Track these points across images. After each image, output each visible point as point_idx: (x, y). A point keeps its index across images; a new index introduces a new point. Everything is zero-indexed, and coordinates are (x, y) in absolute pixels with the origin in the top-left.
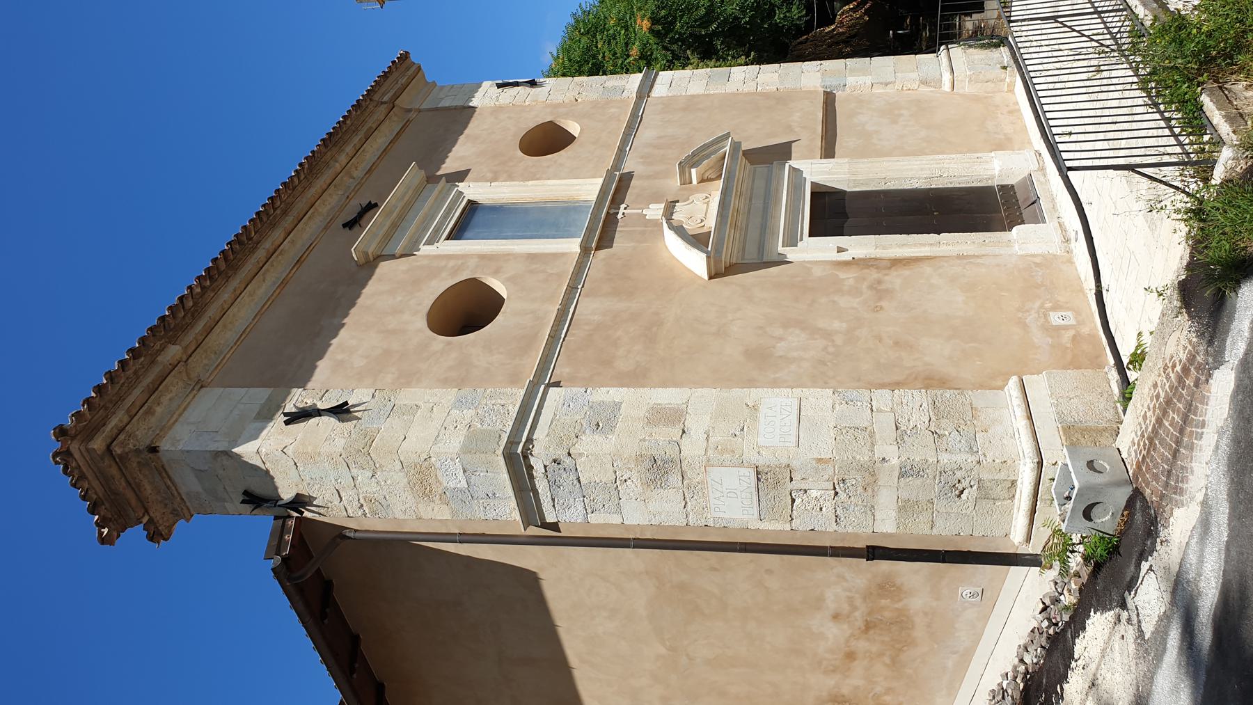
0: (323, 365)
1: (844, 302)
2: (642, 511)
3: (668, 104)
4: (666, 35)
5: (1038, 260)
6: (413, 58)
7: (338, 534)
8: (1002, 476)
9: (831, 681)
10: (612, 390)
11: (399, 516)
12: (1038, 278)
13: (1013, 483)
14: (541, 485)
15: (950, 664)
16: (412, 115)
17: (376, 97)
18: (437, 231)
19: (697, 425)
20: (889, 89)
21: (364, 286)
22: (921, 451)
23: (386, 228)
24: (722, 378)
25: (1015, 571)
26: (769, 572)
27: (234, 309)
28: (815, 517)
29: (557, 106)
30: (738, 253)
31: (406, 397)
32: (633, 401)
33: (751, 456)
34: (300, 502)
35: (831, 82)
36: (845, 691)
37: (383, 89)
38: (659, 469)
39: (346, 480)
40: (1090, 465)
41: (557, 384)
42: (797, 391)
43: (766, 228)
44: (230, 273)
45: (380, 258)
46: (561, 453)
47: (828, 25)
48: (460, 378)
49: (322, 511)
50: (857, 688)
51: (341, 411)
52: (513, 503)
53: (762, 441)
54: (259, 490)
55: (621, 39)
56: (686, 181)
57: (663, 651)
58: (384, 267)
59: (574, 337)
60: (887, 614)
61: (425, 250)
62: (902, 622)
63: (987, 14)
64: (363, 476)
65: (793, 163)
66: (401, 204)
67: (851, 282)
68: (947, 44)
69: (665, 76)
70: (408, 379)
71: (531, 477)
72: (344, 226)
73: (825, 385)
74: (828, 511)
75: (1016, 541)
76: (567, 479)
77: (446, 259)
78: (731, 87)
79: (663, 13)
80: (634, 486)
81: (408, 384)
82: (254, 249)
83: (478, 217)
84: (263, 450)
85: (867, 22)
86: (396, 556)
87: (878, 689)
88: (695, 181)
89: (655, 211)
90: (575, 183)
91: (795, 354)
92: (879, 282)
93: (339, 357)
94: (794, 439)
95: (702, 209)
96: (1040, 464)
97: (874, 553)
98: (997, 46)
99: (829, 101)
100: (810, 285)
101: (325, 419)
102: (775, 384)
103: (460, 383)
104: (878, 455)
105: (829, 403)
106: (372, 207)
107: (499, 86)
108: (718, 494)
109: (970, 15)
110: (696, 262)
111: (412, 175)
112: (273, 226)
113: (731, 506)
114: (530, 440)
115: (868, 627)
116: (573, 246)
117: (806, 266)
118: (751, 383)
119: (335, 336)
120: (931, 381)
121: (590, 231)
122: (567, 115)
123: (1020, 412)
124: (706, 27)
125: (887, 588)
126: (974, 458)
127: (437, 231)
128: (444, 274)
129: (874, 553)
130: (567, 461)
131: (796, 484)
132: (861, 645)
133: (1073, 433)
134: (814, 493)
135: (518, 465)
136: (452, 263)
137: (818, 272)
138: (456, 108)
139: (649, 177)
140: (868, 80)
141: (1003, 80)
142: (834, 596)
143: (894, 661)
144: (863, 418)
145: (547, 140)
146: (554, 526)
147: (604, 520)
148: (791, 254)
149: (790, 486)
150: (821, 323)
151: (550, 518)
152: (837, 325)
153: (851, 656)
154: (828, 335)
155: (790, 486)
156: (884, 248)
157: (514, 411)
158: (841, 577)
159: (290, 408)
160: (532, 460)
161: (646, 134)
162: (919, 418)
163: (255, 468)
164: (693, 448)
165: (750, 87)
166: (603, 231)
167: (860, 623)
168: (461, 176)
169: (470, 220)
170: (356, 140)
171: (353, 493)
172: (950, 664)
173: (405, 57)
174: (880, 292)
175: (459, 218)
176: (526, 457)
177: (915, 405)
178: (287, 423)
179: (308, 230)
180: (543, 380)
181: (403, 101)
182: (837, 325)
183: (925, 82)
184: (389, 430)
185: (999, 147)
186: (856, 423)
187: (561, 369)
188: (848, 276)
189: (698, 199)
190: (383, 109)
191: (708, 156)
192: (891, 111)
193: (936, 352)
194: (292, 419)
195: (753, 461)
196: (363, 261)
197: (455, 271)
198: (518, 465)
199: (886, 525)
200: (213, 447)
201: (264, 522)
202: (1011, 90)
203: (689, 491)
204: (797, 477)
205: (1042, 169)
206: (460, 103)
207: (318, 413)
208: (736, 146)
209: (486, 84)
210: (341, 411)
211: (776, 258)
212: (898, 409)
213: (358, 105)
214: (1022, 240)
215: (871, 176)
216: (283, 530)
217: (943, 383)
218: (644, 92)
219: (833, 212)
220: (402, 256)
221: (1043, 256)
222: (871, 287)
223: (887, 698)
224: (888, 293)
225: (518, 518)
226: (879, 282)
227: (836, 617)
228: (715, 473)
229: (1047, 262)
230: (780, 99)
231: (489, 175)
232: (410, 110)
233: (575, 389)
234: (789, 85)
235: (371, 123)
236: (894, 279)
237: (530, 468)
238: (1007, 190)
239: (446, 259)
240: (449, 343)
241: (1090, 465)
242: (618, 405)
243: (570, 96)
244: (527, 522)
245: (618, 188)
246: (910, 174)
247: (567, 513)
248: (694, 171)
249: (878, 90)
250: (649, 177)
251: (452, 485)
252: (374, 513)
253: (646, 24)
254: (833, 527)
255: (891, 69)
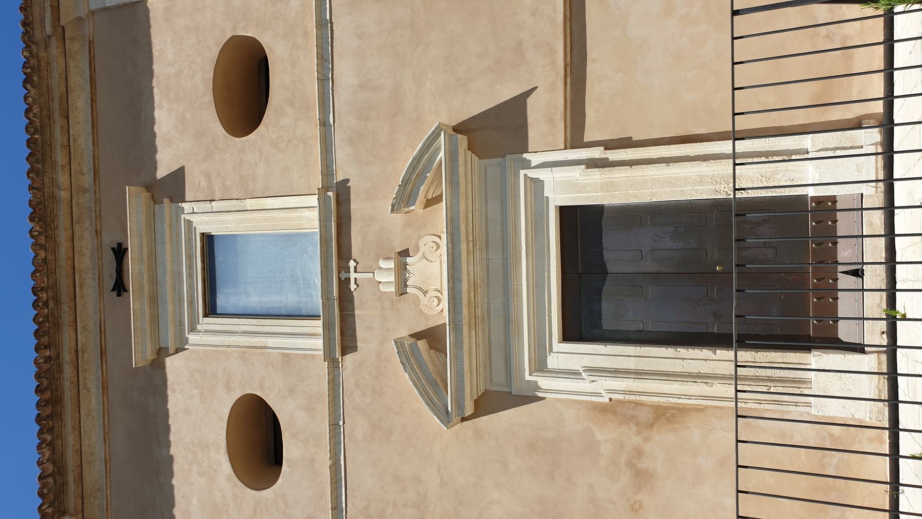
17: (38, 35)
23: (147, 311)
27: (85, 442)
37: (37, 24)
44: (58, 408)
45: (162, 353)
58: (173, 364)
66: (145, 268)
106: (120, 252)
111: (134, 200)
175: (203, 269)
188: (606, 435)
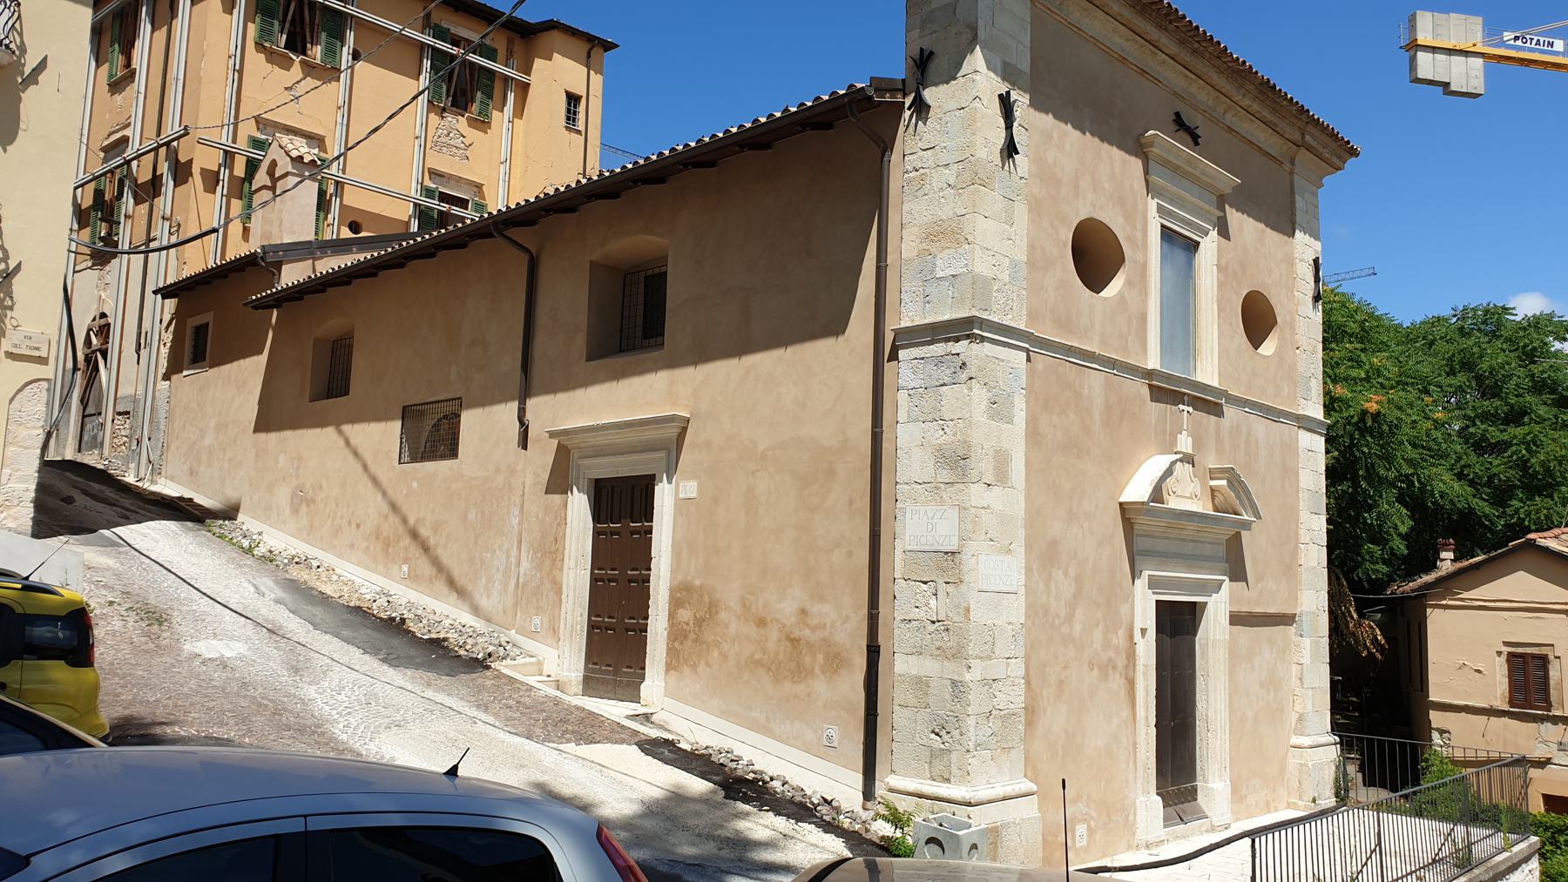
0: (1049, 119)
1: (1098, 634)
2: (910, 442)
3: (1291, 448)
4: (1359, 429)
5: (1131, 818)
6: (1352, 161)
7: (886, 146)
8: (954, 770)
9: (734, 603)
10: (1023, 414)
11: (906, 207)
12: (1118, 818)
13: (948, 780)
14: (938, 349)
15: (755, 714)
16: (1287, 166)
17: (1310, 128)
18: (1170, 214)
19: (994, 498)
20: (1294, 681)
21: (1120, 147)
22: (976, 701)
24: (1033, 518)
25: (858, 779)
26: (850, 554)
28: (908, 603)
29: (1292, 326)
30: (1144, 531)
31: (1021, 211)
32: (1014, 437)
33: (971, 548)
34: (921, 108)
35: (1305, 622)
36: (723, 615)
37: (1317, 133)
38: (956, 461)
39: (944, 158)
40: (974, 847)
41: (1029, 360)
42: (1022, 591)
43: (1165, 557)
46: (972, 370)
47: (1357, 610)
48: (1037, 262)
49: (911, 129)
50: (727, 627)
51: (1010, 149)
52: (919, 321)
53: (983, 558)
54: (933, 67)
55: (1354, 373)
56: (1213, 474)
57: (762, 447)
58: (1136, 164)
59: (1068, 370)
60: (808, 660)
61: (1152, 204)
62: (800, 672)
63: (1362, 790)
64: (949, 175)
65: (1227, 584)
66: (1198, 173)
67: (1115, 641)
68: (1341, 743)
69: (1319, 443)
70: (1035, 208)
71: (947, 340)
72: (1177, 114)
73: (1028, 616)
74: (915, 614)
75: (887, 780)
76: (945, 374)
77: (1141, 227)
78: (1304, 515)
79: (1385, 427)
80: (936, 436)
81: (1030, 211)
82: (1159, 26)
83: (1180, 255)
84: (977, 77)
85: (1359, 654)
86: (868, 200)
87: (726, 647)
88: (1213, 483)
89: (1185, 443)
90: (1213, 360)
91: (1053, 588)
92: (1114, 668)
93: (1055, 135)
94: (984, 588)
95: (1188, 497)
96: (969, 804)
97: (873, 652)
98: (1337, 795)
99: (1286, 619)
100: (1113, 603)
101: (1003, 133)
102: (1029, 570)
103: (1031, 263)
104: (973, 662)
105: (1013, 620)
106: (1195, 139)
107: (1316, 261)
108: (930, 514)
109: (1361, 769)
110: (1137, 490)
111: (1229, 180)
112: (1182, 42)
113: (917, 525)
114: (983, 339)
115: (794, 641)
116: (1153, 362)
117: (1129, 598)
118: (1029, 547)
119: (1075, 127)
120: (1031, 712)
121: (1169, 378)
122: (1282, 339)
123: (1009, 791)
124: (1365, 478)
125: (835, 662)
126: (971, 747)
127: (1170, 214)
128: (1128, 229)
129: (873, 652)
130: (964, 376)
131: (942, 587)
132: (774, 634)
133: (994, 833)
134: (933, 602)
135: (962, 329)
136: (1139, 235)
137: (1124, 609)
138: (1293, 214)
139: (1218, 433)
140: (1306, 660)
141: (1300, 798)
142: (824, 611)
143: (758, 663)
144: (1001, 650)
145: (1257, 319)
146: (894, 357)
147: (901, 405)
148: (1141, 583)
149: (940, 581)
150: (1079, 612)
151: (902, 354)
152: (1078, 627)
153: (762, 623)
154: (1069, 618)
155: (940, 581)
156: (1145, 673)
157: (1007, 321)
158: (846, 620)
159: (1014, 95)
160: (965, 343)
161: (1260, 426)
162: (1001, 700)
163: (959, 66)
164: (977, 494)
165: (1304, 537)
166: (1167, 391)
167: (797, 633)
168: (1224, 232)
169: (1180, 245)
170: (1265, 113)
171: (931, 163)
172: (755, 714)
173: (1353, 153)
174: (1106, 668)
176: (968, 337)
177: (1012, 697)
178: (1000, 96)
179: (1174, 76)
180: (1031, 343)
181: (1303, 156)
182: (1078, 627)
183: (1301, 719)
184: (992, 200)
185: (1235, 790)
186: (998, 644)
187: (1042, 360)
188: (1120, 639)
189: (1193, 487)
190: (1297, 136)
191: (1238, 497)
192: (1273, 683)
193: (1055, 718)
194: (1006, 104)
195: (965, 550)
196: (1143, 141)
197: (1130, 239)
198: (962, 329)
199: (901, 665)
200: (981, 24)
201: (898, 70)
202: (1289, 806)
203: (934, 489)
204: (950, 588)
205: (1213, 829)
206: (1298, 219)
207: (1009, 127)
208: (1247, 525)
209: (1318, 245)
210: (1010, 149)
211: (1137, 568)
212: (1009, 682)
213: (1303, 111)
214: (1149, 805)
215: (1211, 661)
216: (893, 91)
217: (1029, 725)
218: (1305, 423)
219: (1177, 622)
220: (1147, 181)
221: (1135, 822)
222: (1110, 660)
223: (716, 654)
224: (1105, 676)
225: (903, 325)
226: (1114, 668)
227: (803, 612)
228: (953, 514)
229: (1129, 827)
230: (1290, 568)
231: (1223, 262)
232: (1293, 163)
233: (1024, 378)
234: (1305, 577)
235: (1282, 126)
236: (1117, 682)
237: (957, 340)
238: (1192, 794)
239: (1141, 227)
240: (1065, 245)
241: (974, 847)
242: (1011, 422)
243: (1302, 340)
244: (898, 333)
245: (1208, 403)
246: (1212, 701)
247: (908, 369)
248: (1224, 482)
249: (1295, 669)
250: (1218, 433)
251: (939, 262)
252: (909, 181)
253: (1373, 407)
254: (899, 617)
255: (1317, 684)
